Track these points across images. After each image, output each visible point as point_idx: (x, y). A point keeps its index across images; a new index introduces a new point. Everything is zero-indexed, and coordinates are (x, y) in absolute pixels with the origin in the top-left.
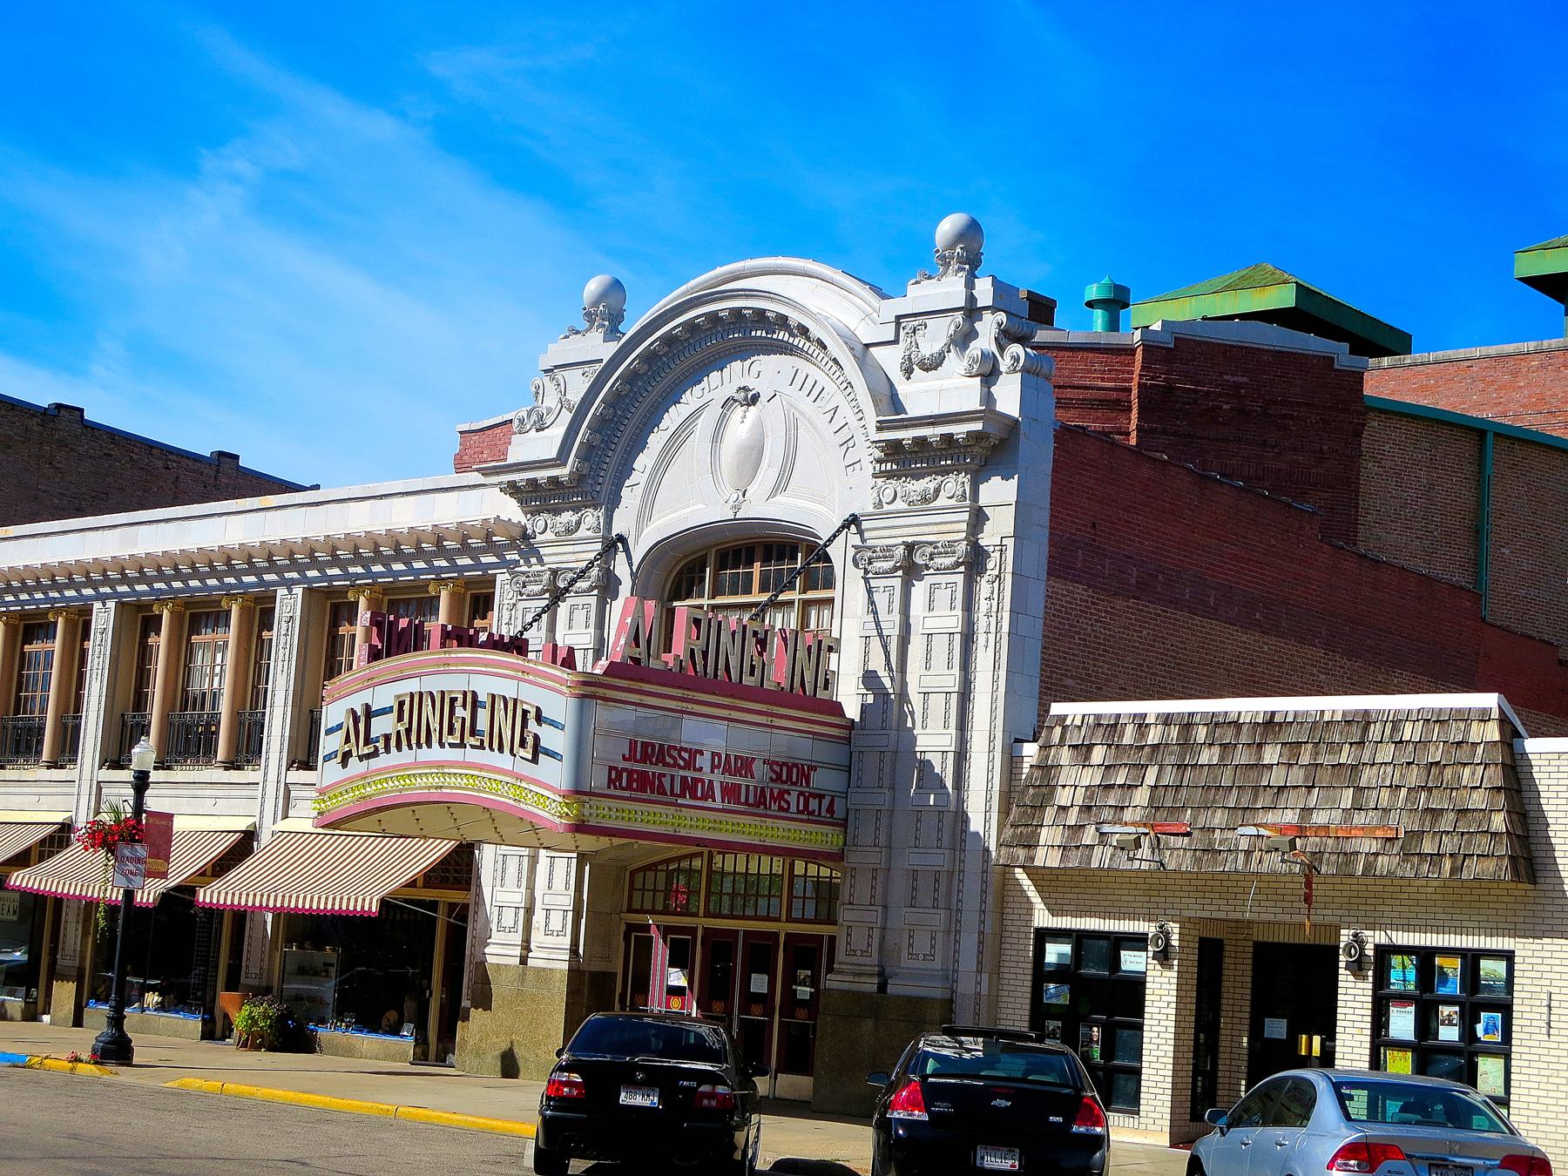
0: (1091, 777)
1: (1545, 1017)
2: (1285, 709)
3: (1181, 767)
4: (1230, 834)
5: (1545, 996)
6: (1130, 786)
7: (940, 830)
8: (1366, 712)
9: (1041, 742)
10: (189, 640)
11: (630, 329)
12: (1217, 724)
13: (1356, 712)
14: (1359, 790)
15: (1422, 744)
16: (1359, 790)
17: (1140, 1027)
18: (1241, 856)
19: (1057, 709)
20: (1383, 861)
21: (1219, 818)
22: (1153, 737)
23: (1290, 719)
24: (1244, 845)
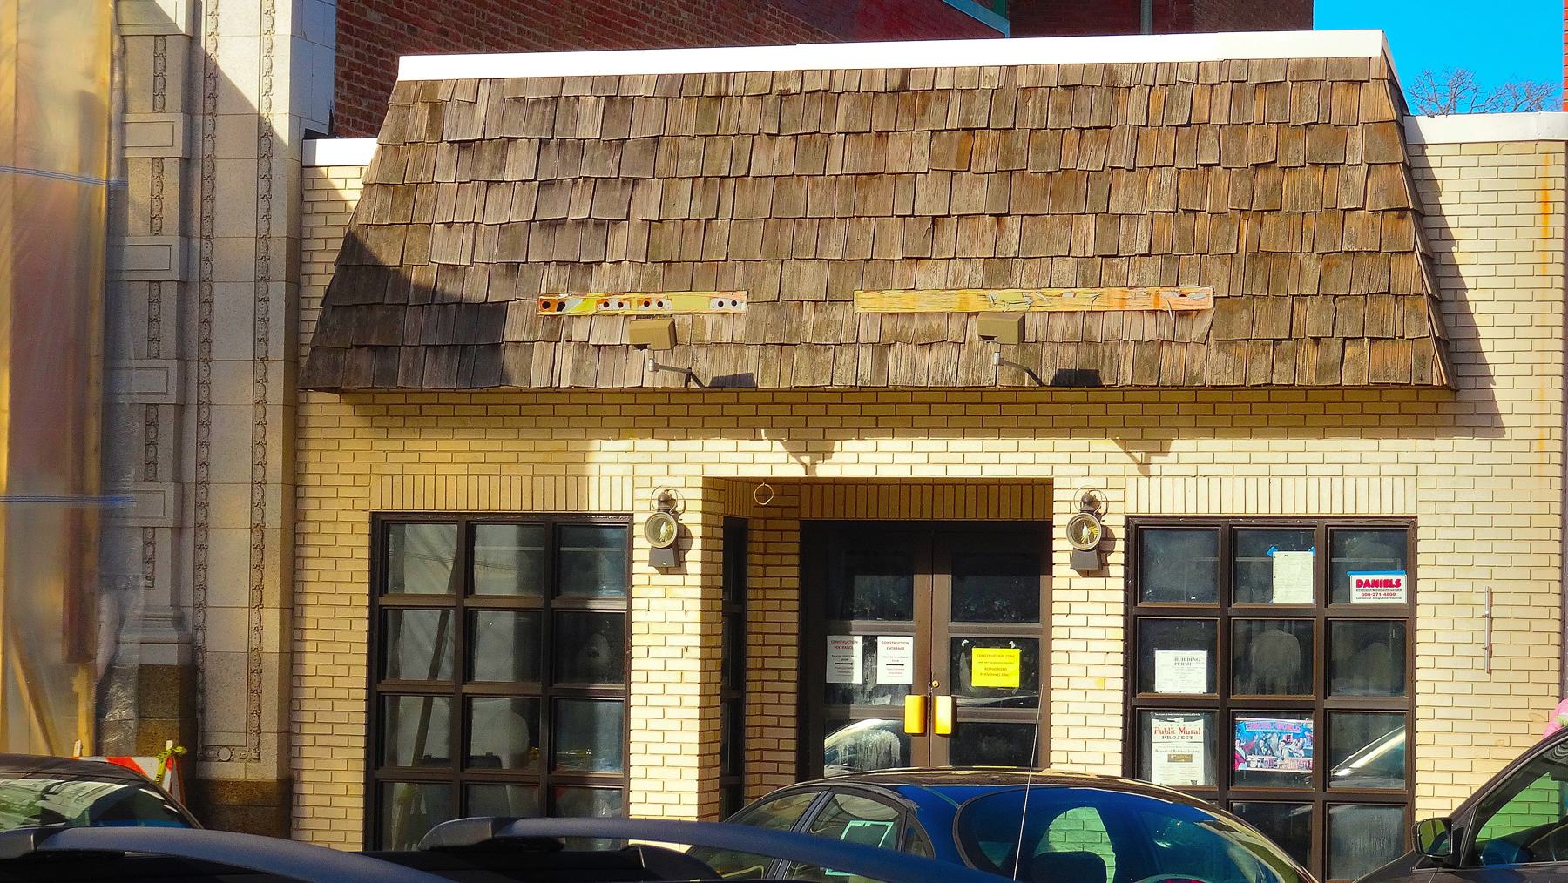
0: (507, 208)
1: (1483, 637)
2: (931, 64)
3: (711, 183)
4: (839, 313)
5: (1483, 599)
6: (599, 223)
7: (153, 320)
8: (1109, 69)
9: (385, 133)
10: (812, 658)
11: (41, 784)
12: (784, 95)
13: (1088, 68)
14: (1110, 219)
15: (1233, 130)
16: (1110, 219)
17: (627, 694)
18: (866, 354)
19: (413, 68)
20: (1171, 356)
21: (809, 281)
22: (644, 125)
23: (943, 84)
24: (869, 334)
